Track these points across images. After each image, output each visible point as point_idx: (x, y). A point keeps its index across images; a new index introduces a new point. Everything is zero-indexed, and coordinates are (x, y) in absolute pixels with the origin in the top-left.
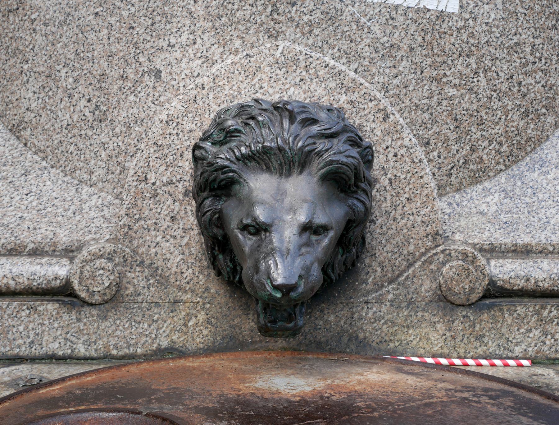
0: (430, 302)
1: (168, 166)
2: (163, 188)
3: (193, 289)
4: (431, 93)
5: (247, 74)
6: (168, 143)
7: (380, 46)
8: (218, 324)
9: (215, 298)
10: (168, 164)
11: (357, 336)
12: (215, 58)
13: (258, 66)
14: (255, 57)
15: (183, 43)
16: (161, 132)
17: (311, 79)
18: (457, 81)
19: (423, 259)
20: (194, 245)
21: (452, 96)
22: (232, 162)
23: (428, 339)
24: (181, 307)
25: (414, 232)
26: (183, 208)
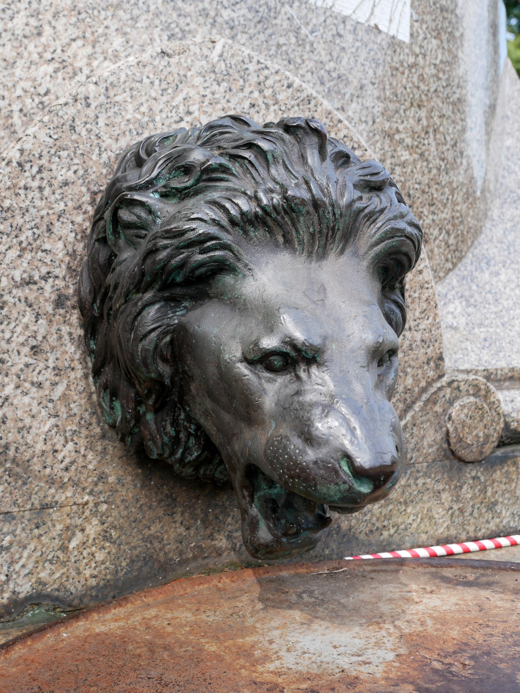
0: (434, 461)
1: (23, 250)
2: (14, 291)
3: (76, 479)
4: (384, 155)
5: (164, 85)
6: (23, 205)
7: (325, 75)
8: (123, 537)
9: (117, 491)
10: (24, 245)
11: (339, 527)
12: (78, 64)
13: (182, 73)
14: (177, 57)
15: (16, 32)
16: (9, 183)
17: (267, 105)
18: (408, 141)
19: (424, 397)
20: (76, 398)
21: (404, 162)
22: (222, 227)
23: (431, 518)
24: (54, 517)
25: (412, 356)
26: (53, 330)
